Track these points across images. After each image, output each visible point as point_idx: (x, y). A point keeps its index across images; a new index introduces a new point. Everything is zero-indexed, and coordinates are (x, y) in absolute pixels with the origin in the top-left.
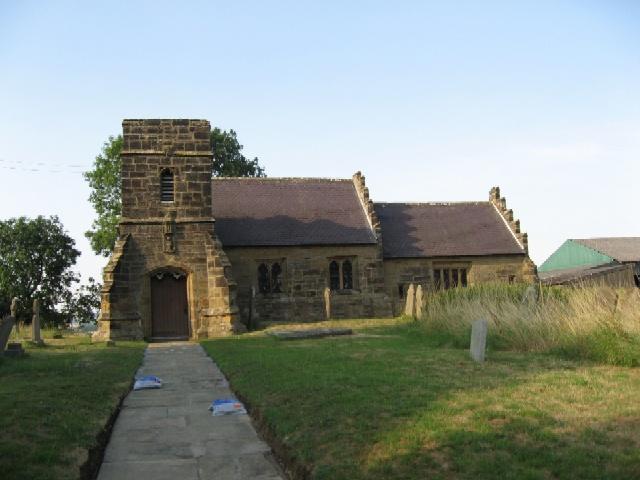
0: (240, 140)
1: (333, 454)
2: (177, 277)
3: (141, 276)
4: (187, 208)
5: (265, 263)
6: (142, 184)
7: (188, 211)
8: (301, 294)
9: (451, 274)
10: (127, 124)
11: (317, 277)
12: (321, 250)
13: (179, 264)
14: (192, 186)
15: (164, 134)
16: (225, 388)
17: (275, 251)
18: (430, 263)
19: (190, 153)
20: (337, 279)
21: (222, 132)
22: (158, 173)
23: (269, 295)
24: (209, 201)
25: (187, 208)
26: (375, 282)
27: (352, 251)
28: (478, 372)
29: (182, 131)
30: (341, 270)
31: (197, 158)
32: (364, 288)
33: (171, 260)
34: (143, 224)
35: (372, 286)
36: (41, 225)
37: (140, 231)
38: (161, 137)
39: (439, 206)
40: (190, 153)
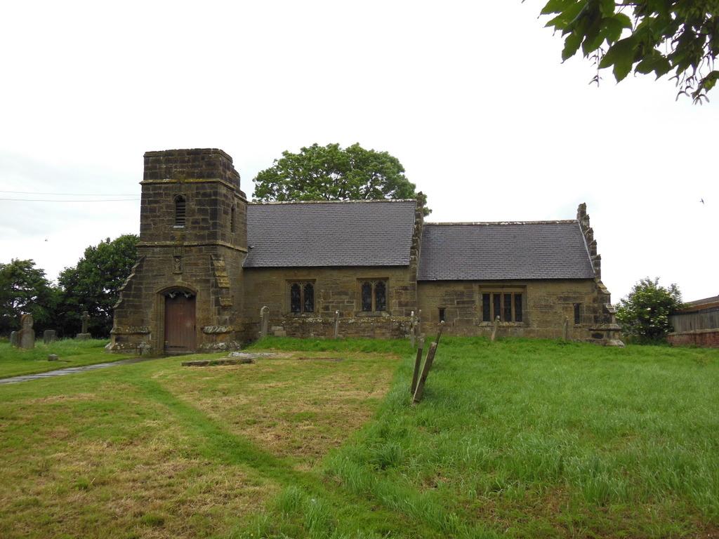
0: (399, 160)
1: (228, 515)
2: (187, 296)
3: (153, 295)
4: (194, 232)
9: (491, 298)
10: (285, 154)
11: (346, 298)
13: (186, 284)
15: (178, 164)
17: (305, 273)
18: (476, 287)
19: (201, 180)
21: (375, 152)
22: (171, 200)
23: (299, 314)
25: (194, 232)
27: (383, 274)
30: (373, 292)
31: (206, 185)
32: (395, 311)
33: (179, 281)
34: (156, 246)
37: (153, 253)
38: (176, 167)
39: (512, 224)
40: (201, 180)
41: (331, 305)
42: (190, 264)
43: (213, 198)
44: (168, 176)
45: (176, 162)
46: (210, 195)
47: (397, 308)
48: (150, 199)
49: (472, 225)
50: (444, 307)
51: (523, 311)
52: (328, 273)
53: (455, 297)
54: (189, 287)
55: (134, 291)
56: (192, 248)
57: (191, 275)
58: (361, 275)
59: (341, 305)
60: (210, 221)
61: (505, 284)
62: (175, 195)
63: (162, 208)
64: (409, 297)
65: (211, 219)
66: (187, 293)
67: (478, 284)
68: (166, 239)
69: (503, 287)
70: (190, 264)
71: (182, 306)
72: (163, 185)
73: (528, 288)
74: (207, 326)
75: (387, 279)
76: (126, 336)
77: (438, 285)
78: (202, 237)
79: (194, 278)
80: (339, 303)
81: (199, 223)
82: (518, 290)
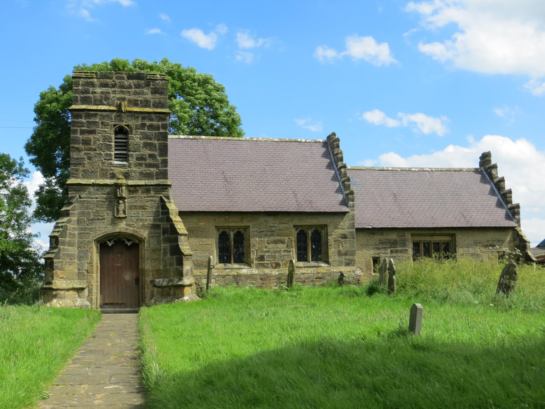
2: (129, 244)
5: (227, 231)
6: (92, 143)
7: (141, 173)
8: (264, 266)
12: (287, 219)
13: (130, 230)
14: (146, 145)
16: (50, 305)
18: (408, 236)
20: (306, 249)
24: (165, 163)
26: (346, 254)
28: (199, 290)
29: (138, 86)
35: (343, 258)
36: (483, 154)
38: (114, 92)
41: (266, 254)
42: (135, 207)
43: (162, 131)
44: (105, 103)
45: (114, 86)
46: (158, 128)
47: (337, 258)
48: (83, 128)
49: (384, 170)
50: (377, 256)
51: (330, 260)
52: (262, 219)
53: (388, 246)
54: (135, 234)
55: (69, 238)
56: (138, 188)
57: (137, 220)
58: (297, 222)
59: (277, 254)
60: (158, 158)
61: (436, 232)
62: (115, 125)
63: (99, 140)
64: (348, 245)
65: (160, 156)
66: (129, 241)
67: (410, 232)
68: (104, 176)
69: (432, 235)
70: (135, 207)
71: (119, 255)
72: (99, 113)
73: (457, 237)
74: (158, 278)
75: (325, 226)
76: (62, 292)
77: (372, 233)
78: (149, 176)
79: (141, 224)
80: (276, 252)
81: (145, 159)
82: (447, 239)
